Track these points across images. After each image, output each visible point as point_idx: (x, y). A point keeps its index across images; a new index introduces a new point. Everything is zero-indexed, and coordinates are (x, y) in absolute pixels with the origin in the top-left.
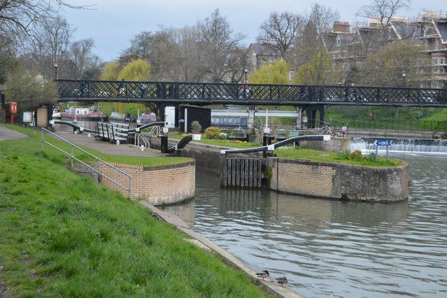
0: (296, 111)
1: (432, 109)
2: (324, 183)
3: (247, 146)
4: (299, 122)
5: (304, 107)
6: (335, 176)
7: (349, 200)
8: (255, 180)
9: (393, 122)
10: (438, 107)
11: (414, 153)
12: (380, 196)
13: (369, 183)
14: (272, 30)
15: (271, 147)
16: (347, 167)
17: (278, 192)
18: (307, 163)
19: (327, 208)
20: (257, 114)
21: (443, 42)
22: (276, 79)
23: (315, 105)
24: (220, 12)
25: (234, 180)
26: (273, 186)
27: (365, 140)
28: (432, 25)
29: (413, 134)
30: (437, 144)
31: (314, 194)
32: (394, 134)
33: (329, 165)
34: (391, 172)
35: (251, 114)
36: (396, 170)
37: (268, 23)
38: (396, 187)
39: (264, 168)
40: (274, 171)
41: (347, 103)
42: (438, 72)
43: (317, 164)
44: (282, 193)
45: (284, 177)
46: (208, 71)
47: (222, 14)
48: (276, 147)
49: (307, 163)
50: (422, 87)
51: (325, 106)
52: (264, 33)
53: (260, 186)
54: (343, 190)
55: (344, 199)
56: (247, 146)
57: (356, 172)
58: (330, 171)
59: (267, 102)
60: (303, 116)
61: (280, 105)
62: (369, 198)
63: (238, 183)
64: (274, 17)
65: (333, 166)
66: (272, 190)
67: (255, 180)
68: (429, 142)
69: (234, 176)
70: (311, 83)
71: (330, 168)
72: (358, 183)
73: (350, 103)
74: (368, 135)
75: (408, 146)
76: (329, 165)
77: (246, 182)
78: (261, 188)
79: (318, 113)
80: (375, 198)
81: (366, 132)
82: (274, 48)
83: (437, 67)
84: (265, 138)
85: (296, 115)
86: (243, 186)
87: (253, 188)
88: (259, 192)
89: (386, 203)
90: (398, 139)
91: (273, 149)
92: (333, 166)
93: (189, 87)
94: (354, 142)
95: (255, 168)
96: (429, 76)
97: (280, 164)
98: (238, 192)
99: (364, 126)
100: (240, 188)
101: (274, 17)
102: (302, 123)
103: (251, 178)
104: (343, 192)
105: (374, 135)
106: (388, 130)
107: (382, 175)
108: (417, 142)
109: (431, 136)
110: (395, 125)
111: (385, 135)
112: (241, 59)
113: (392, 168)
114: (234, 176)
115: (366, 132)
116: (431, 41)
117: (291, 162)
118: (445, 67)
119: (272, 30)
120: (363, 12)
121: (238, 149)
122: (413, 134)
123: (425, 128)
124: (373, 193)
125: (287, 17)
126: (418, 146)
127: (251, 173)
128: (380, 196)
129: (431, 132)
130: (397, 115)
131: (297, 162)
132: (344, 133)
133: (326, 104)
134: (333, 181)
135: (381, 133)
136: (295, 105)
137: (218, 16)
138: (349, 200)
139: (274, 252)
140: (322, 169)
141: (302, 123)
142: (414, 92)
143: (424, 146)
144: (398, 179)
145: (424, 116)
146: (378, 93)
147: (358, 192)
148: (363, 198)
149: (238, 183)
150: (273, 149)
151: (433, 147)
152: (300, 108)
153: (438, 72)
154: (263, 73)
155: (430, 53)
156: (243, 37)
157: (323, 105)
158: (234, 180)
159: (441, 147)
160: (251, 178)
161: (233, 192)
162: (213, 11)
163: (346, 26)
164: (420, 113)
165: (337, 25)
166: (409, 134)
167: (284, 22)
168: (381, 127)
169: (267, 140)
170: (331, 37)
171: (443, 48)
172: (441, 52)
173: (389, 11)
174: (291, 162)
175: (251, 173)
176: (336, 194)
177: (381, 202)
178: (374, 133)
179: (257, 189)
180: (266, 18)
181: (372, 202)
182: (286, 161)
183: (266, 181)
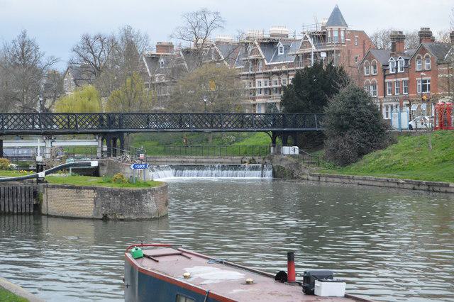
0: (95, 140)
1: (245, 134)
2: (86, 205)
3: (26, 174)
4: (99, 150)
5: (104, 136)
6: (97, 198)
7: (109, 219)
8: (28, 206)
9: (202, 148)
10: (240, 131)
11: (214, 179)
12: (136, 214)
13: (126, 204)
14: (85, 53)
15: (42, 174)
16: (106, 189)
17: (48, 216)
18: (71, 187)
19: (89, 228)
20: (54, 144)
21: (267, 63)
22: (84, 106)
23: (114, 132)
24: (28, 34)
25: (7, 207)
26: (44, 211)
27: (172, 167)
28: (255, 46)
29: (222, 160)
30: (244, 168)
31: (79, 216)
32: (204, 160)
33: (91, 188)
34: (145, 192)
35: (48, 144)
36: (150, 190)
37: (81, 45)
38: (151, 205)
39: (36, 194)
40: (44, 197)
41: (149, 130)
42: (262, 94)
43: (80, 188)
44: (51, 216)
45: (54, 202)
46: (15, 98)
47: (30, 36)
48: (46, 173)
49: (71, 187)
50: (247, 111)
51: (125, 134)
52: (76, 57)
53: (32, 211)
54: (103, 211)
55: (105, 219)
56: (26, 174)
57: (115, 193)
58: (92, 194)
59: (64, 131)
60: (102, 144)
61: (77, 133)
62: (126, 217)
63: (11, 210)
64: (87, 39)
65: (94, 189)
66: (44, 215)
67: (28, 206)
68: (236, 167)
69: (7, 203)
70: (120, 109)
71: (92, 191)
72: (116, 203)
73: (151, 130)
74: (179, 162)
75: (214, 172)
76: (91, 188)
77: (19, 208)
78: (34, 214)
79: (118, 141)
80: (132, 217)
81: (177, 160)
82: (87, 71)
83: (261, 89)
84: (38, 166)
85: (96, 144)
86: (16, 212)
87: (26, 214)
88: (32, 217)
89: (142, 220)
90: (205, 165)
91: (44, 176)
92: (94, 189)
93: (18, 117)
94: (160, 169)
95: (27, 195)
96: (254, 99)
97: (49, 190)
98: (11, 218)
99: (174, 153)
100: (13, 214)
101: (87, 39)
102: (102, 151)
103: (23, 205)
104: (103, 213)
105: (185, 162)
106: (198, 157)
107: (137, 195)
108: (223, 168)
109: (240, 161)
110: (205, 151)
111: (196, 162)
112: (56, 85)
113: (146, 188)
114: (7, 203)
115: (177, 160)
116: (255, 62)
117: (58, 187)
118: (448, 81)
119: (85, 53)
120: (177, 33)
121: (9, 178)
122: (222, 160)
123: (234, 154)
124: (130, 212)
125: (99, 38)
126: (225, 172)
127: (23, 200)
128: (136, 214)
129: (240, 157)
130: (210, 141)
131: (63, 187)
132: (142, 160)
133: (125, 132)
134: (95, 203)
135: (191, 159)
136: (95, 134)
137: (26, 39)
138: (109, 219)
139: (77, 278)
140: (84, 192)
141: (102, 151)
142: (58, 117)
143: (230, 172)
144: (153, 198)
145: (237, 141)
146: (179, 119)
147: (117, 212)
148: (121, 217)
149: (11, 210)
150: (44, 176)
151: (240, 172)
152: (99, 137)
153: (262, 94)
154: (73, 99)
155: (254, 75)
156: (56, 60)
157: (123, 132)
158: (7, 207)
159: (248, 172)
160: (23, 205)
161: (7, 218)
162: (19, 33)
163: (169, 47)
164: (233, 138)
165: (160, 47)
166: (218, 160)
167: (97, 44)
168: (191, 154)
169: (39, 168)
170: (154, 59)
171: (266, 69)
172: (265, 73)
173: (204, 32)
174: (58, 187)
175: (23, 200)
176: (98, 214)
177: (137, 220)
178: (185, 160)
179: (30, 214)
180: (77, 40)
181: (129, 220)
182: (53, 187)
183: (37, 207)
